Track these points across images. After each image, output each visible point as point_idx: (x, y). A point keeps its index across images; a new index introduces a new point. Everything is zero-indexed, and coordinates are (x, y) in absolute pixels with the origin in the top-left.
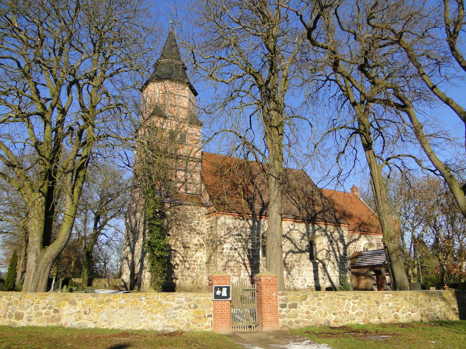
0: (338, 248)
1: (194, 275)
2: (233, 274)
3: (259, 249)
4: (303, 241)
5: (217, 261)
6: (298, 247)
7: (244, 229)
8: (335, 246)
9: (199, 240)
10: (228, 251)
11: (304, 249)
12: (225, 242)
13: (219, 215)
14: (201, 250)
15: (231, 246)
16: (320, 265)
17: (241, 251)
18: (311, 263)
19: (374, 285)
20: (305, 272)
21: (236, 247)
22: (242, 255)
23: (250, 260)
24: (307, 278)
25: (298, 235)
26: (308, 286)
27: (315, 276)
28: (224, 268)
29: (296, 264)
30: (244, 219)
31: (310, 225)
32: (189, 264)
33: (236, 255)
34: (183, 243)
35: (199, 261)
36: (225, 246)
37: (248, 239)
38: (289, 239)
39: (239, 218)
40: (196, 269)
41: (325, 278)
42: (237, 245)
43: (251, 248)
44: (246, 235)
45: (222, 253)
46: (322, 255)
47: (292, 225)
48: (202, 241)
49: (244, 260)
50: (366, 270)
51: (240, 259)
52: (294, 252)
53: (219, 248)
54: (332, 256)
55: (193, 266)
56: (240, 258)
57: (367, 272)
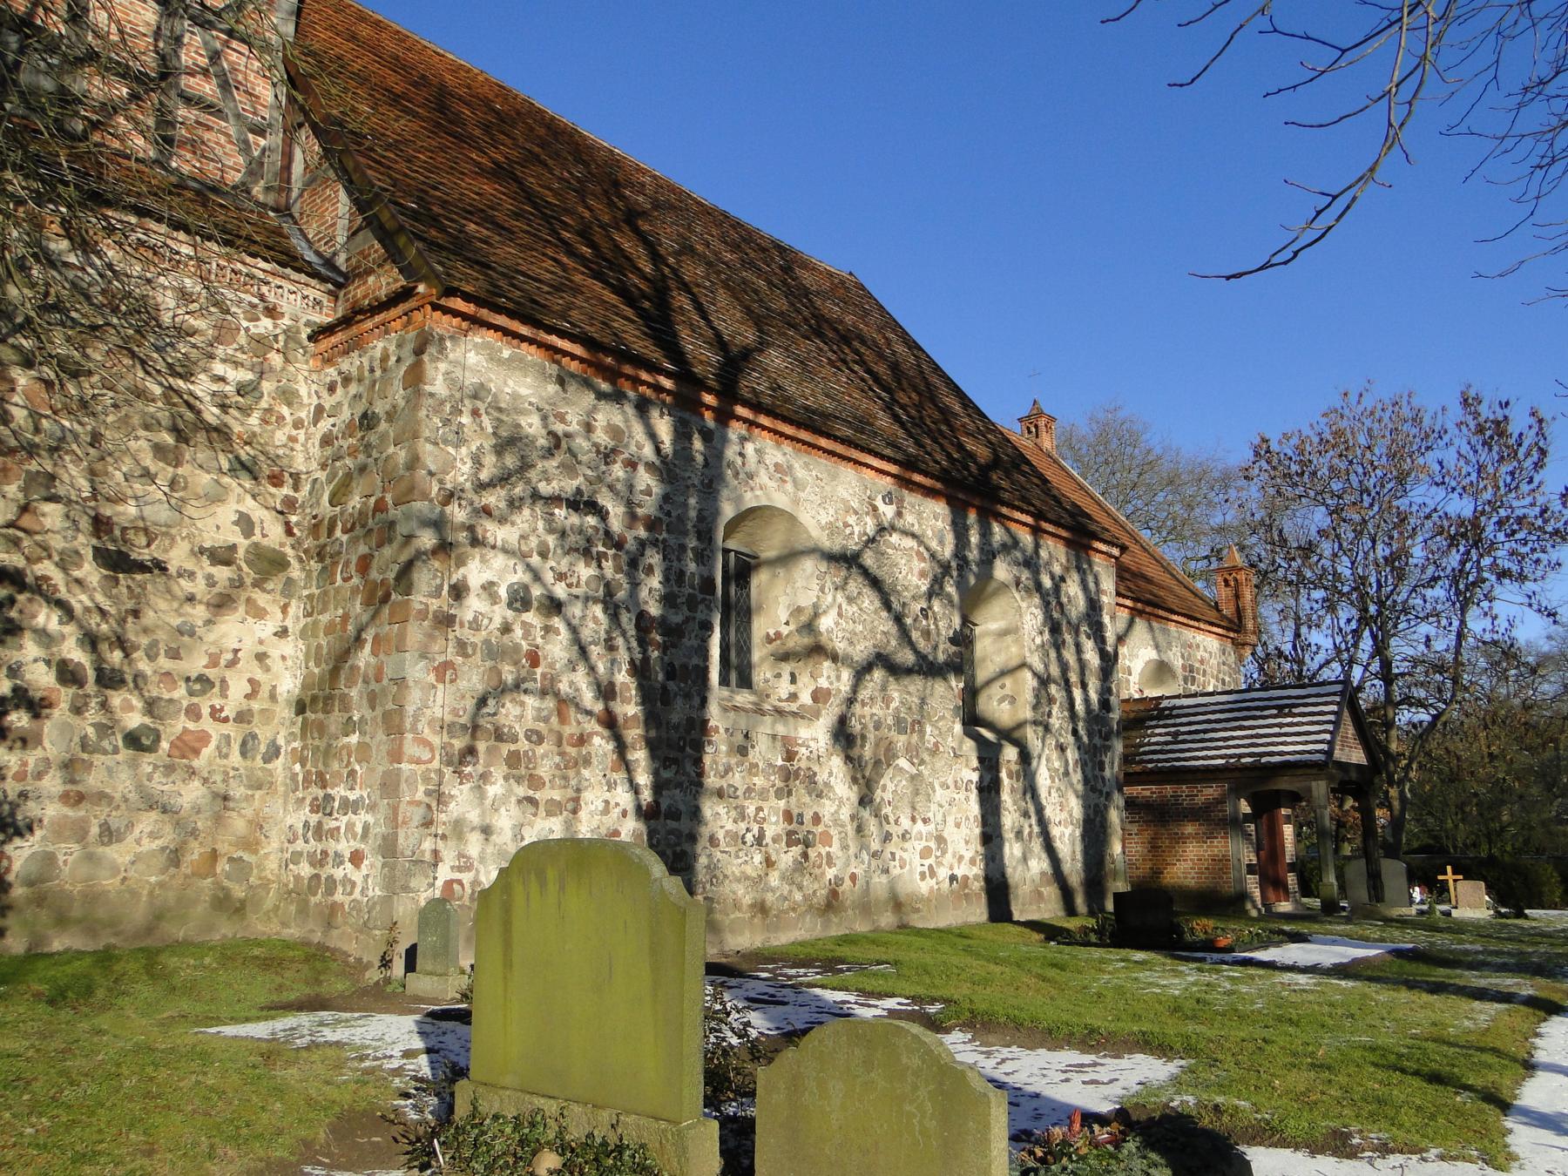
0: (1082, 665)
1: (191, 794)
2: (521, 791)
3: (707, 627)
4: (937, 606)
5: (400, 682)
6: (915, 635)
7: (618, 471)
8: (1069, 656)
9: (245, 523)
10: (500, 613)
11: (941, 657)
12: (476, 542)
13: (442, 324)
14: (261, 598)
15: (521, 576)
16: (1010, 753)
17: (595, 620)
18: (969, 746)
19: (1251, 869)
20: (940, 795)
21: (560, 591)
22: (595, 651)
23: (649, 696)
24: (950, 832)
25: (918, 565)
26: (953, 878)
27: (985, 822)
28: (459, 744)
29: (901, 741)
30: (617, 397)
31: (972, 517)
32: (151, 706)
33: (557, 649)
34: (100, 525)
35: (238, 688)
36: (475, 572)
37: (642, 544)
38: (875, 583)
39: (587, 384)
40: (208, 751)
41: (1026, 831)
42: (561, 577)
43: (654, 610)
44: (632, 517)
45: (446, 621)
46: (1013, 700)
47: (888, 498)
48: (272, 534)
49: (606, 692)
50: (1210, 792)
51: (579, 684)
52: (895, 670)
53: (423, 578)
54: (1055, 710)
55: (182, 723)
56: (581, 678)
57: (1220, 801)
